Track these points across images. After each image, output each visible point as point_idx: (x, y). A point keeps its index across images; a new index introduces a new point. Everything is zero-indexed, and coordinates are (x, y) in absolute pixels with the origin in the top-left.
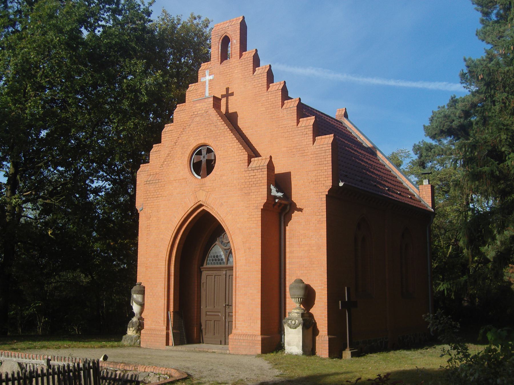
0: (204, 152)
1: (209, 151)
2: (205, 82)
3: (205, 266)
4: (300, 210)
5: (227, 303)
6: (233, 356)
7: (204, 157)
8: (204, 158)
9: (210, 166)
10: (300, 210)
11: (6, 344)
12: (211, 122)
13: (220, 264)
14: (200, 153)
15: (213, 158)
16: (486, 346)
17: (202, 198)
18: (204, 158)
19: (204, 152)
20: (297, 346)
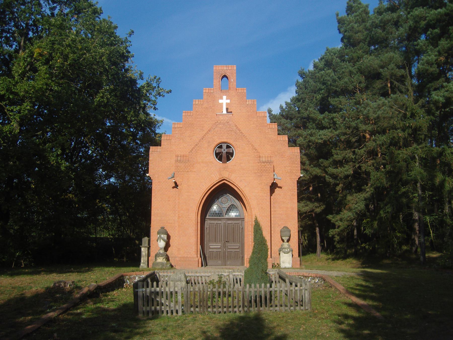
0: (224, 146)
1: (228, 147)
2: (222, 104)
3: (207, 217)
4: (281, 188)
5: (226, 240)
6: (289, 270)
7: (224, 150)
8: (224, 150)
9: (229, 156)
10: (281, 188)
11: (333, 270)
12: (231, 130)
13: (220, 216)
14: (221, 147)
15: (231, 152)
16: (440, 254)
17: (226, 175)
18: (224, 150)
19: (224, 146)
20: (289, 263)
